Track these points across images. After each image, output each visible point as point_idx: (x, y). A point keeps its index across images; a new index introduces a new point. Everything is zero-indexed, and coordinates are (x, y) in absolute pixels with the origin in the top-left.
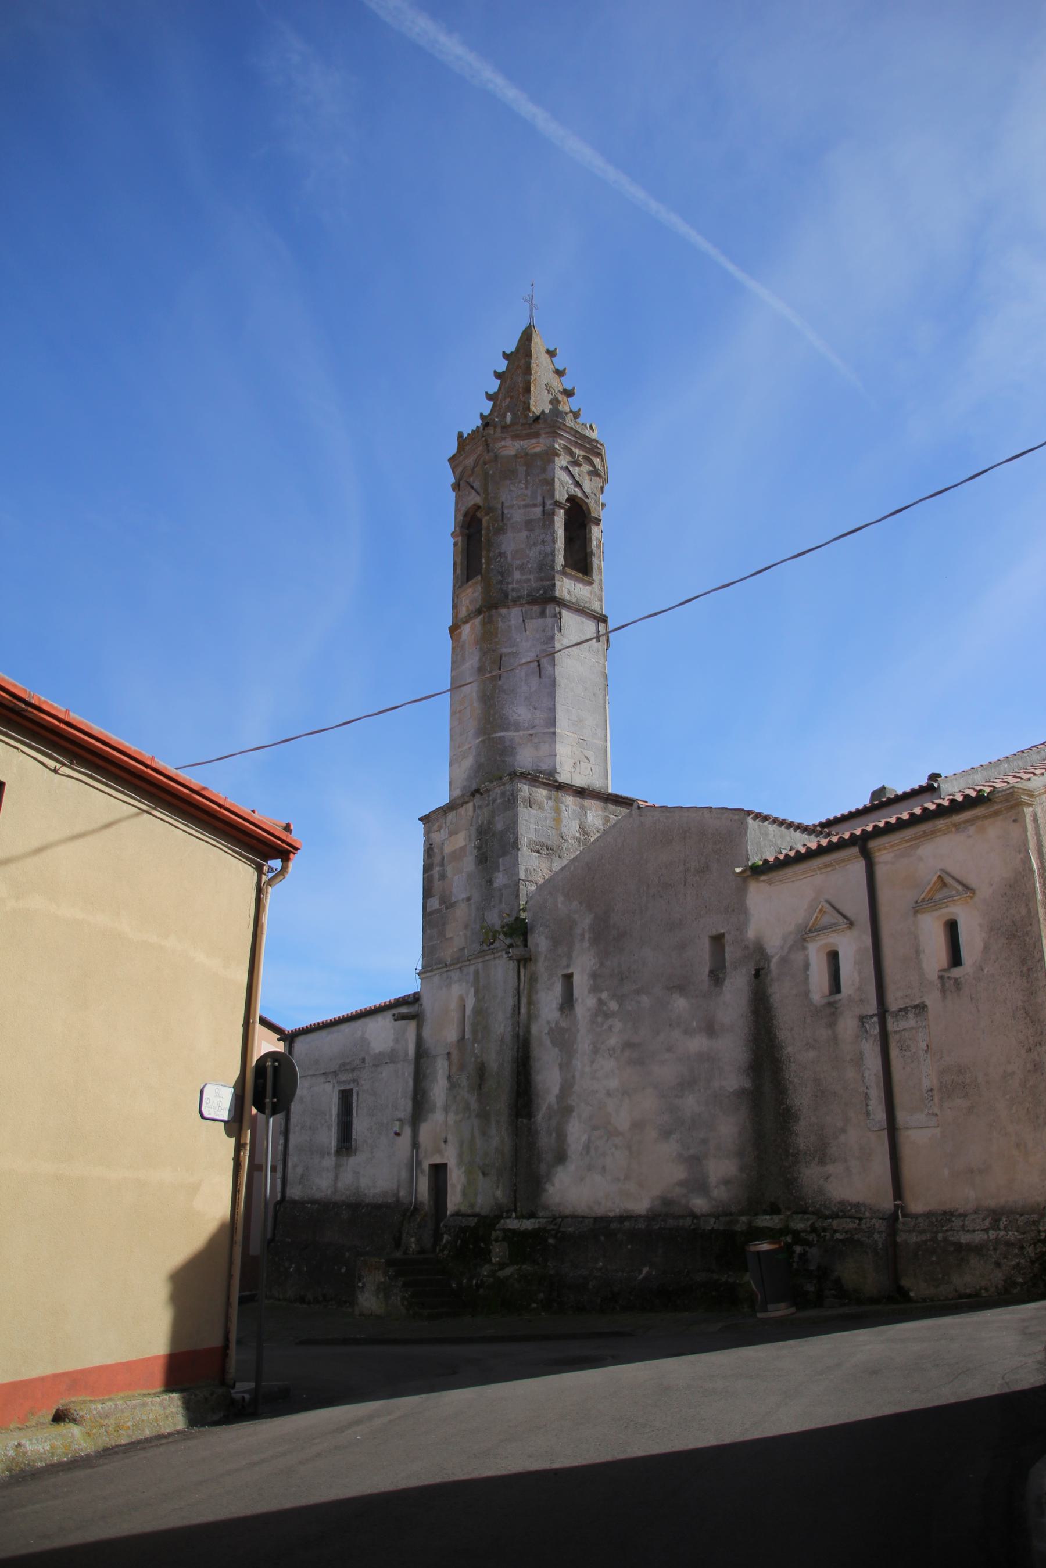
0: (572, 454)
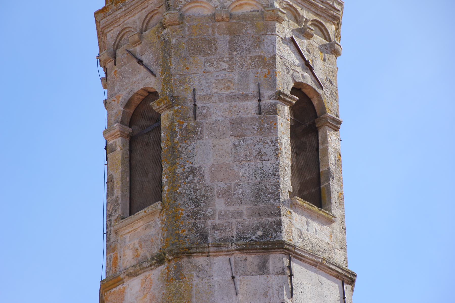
0: (297, 18)
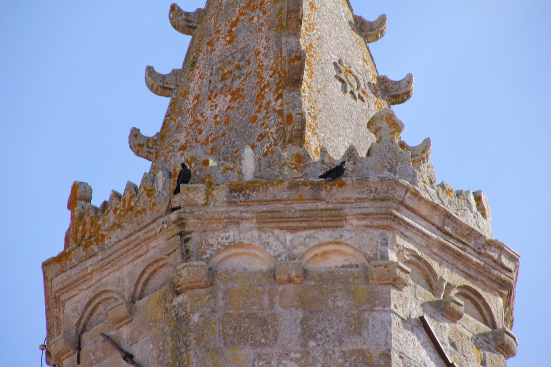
0: (431, 281)
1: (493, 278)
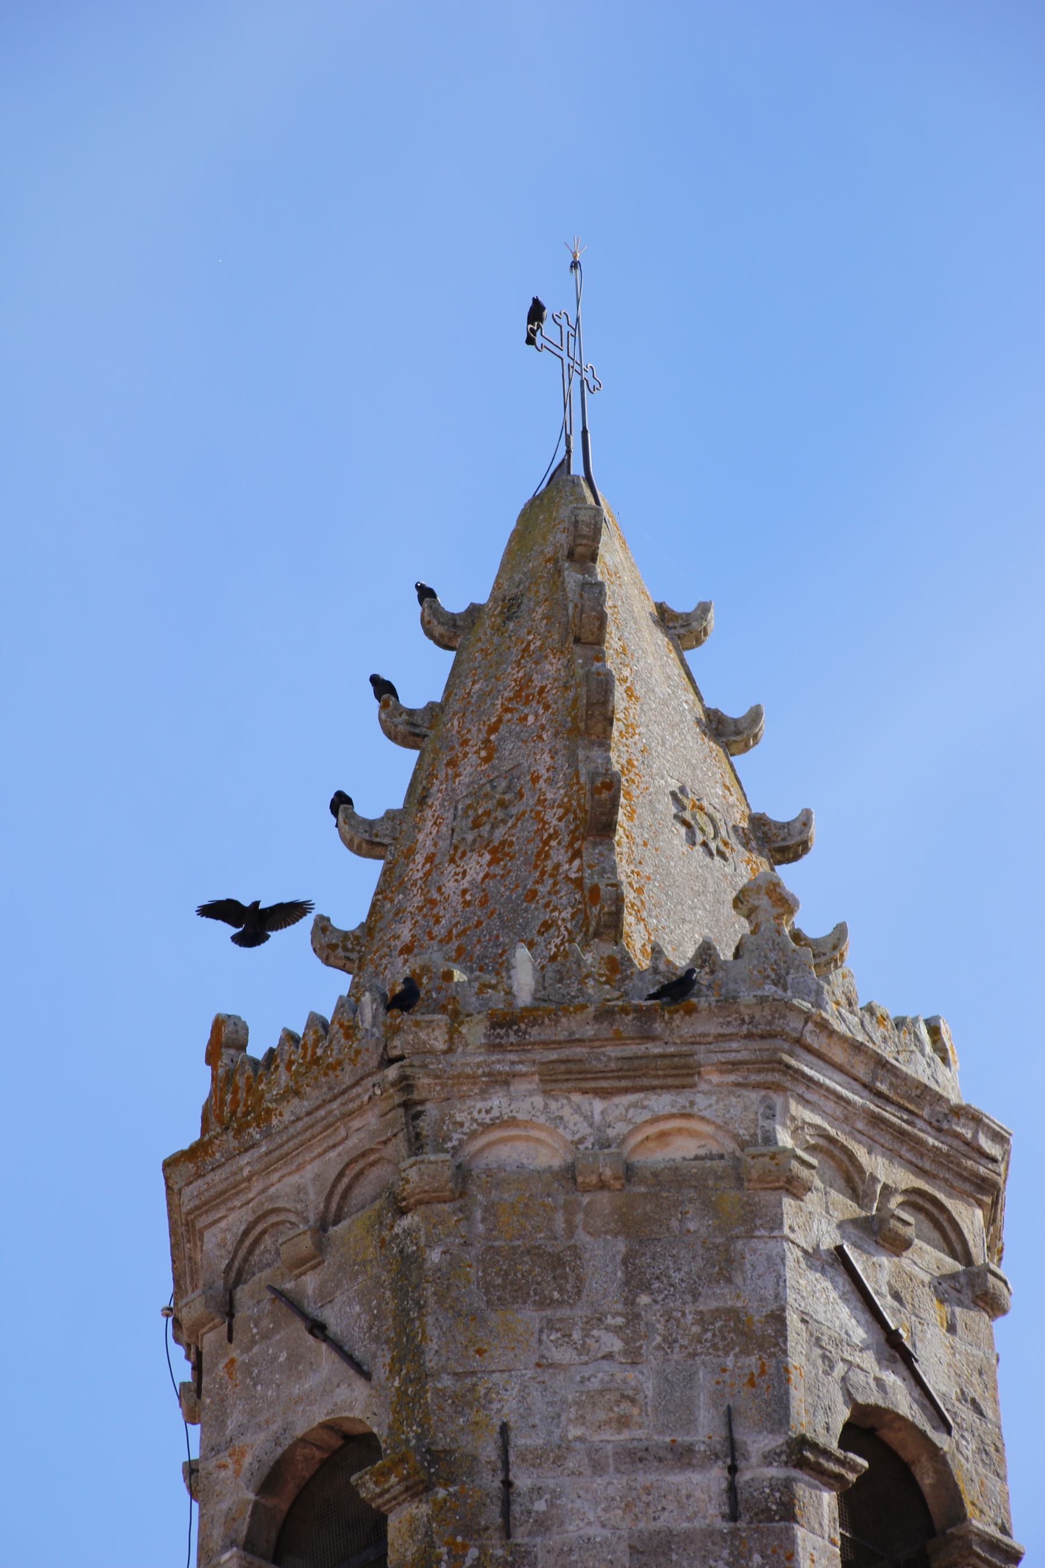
0: (853, 1181)
1: (965, 1173)
